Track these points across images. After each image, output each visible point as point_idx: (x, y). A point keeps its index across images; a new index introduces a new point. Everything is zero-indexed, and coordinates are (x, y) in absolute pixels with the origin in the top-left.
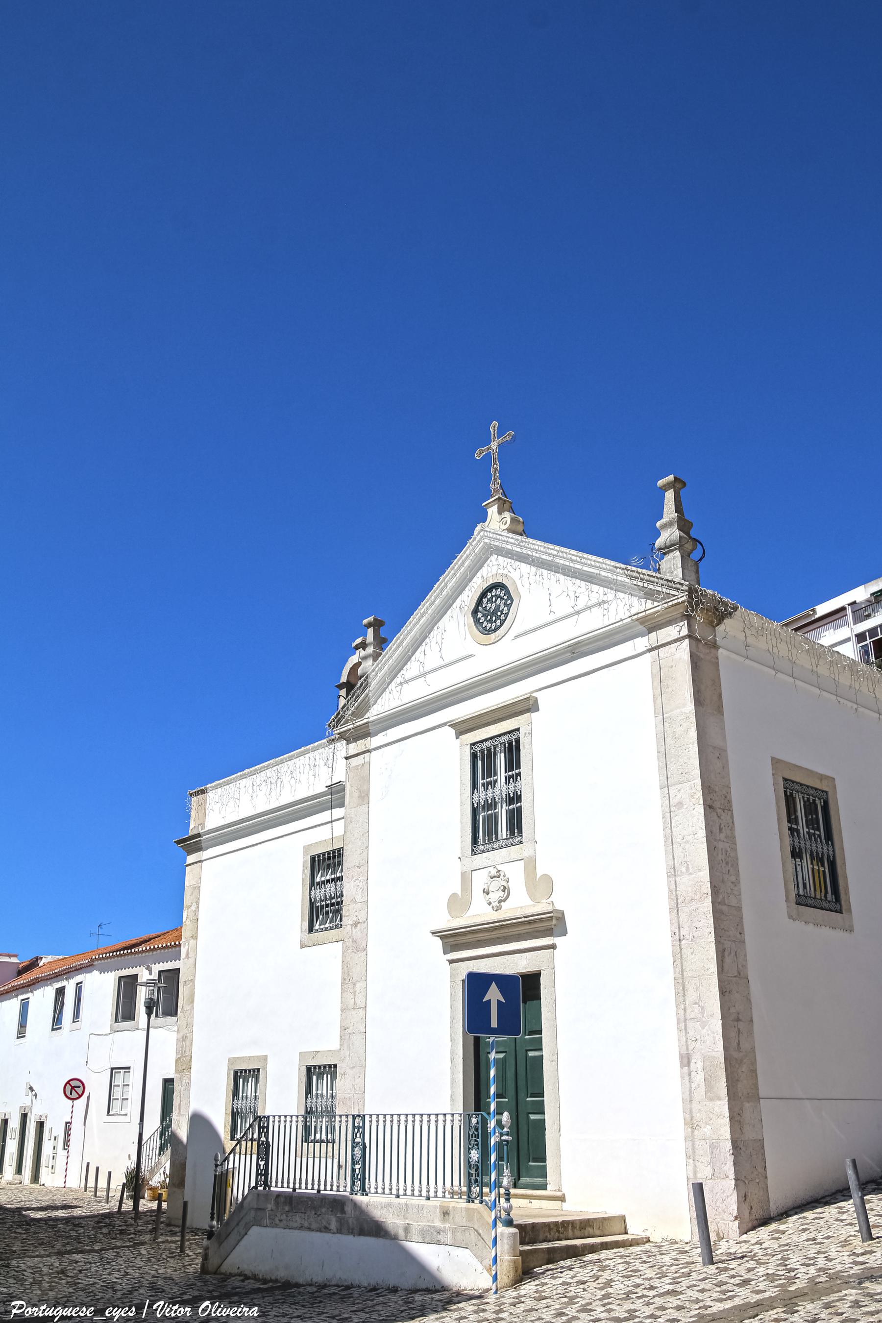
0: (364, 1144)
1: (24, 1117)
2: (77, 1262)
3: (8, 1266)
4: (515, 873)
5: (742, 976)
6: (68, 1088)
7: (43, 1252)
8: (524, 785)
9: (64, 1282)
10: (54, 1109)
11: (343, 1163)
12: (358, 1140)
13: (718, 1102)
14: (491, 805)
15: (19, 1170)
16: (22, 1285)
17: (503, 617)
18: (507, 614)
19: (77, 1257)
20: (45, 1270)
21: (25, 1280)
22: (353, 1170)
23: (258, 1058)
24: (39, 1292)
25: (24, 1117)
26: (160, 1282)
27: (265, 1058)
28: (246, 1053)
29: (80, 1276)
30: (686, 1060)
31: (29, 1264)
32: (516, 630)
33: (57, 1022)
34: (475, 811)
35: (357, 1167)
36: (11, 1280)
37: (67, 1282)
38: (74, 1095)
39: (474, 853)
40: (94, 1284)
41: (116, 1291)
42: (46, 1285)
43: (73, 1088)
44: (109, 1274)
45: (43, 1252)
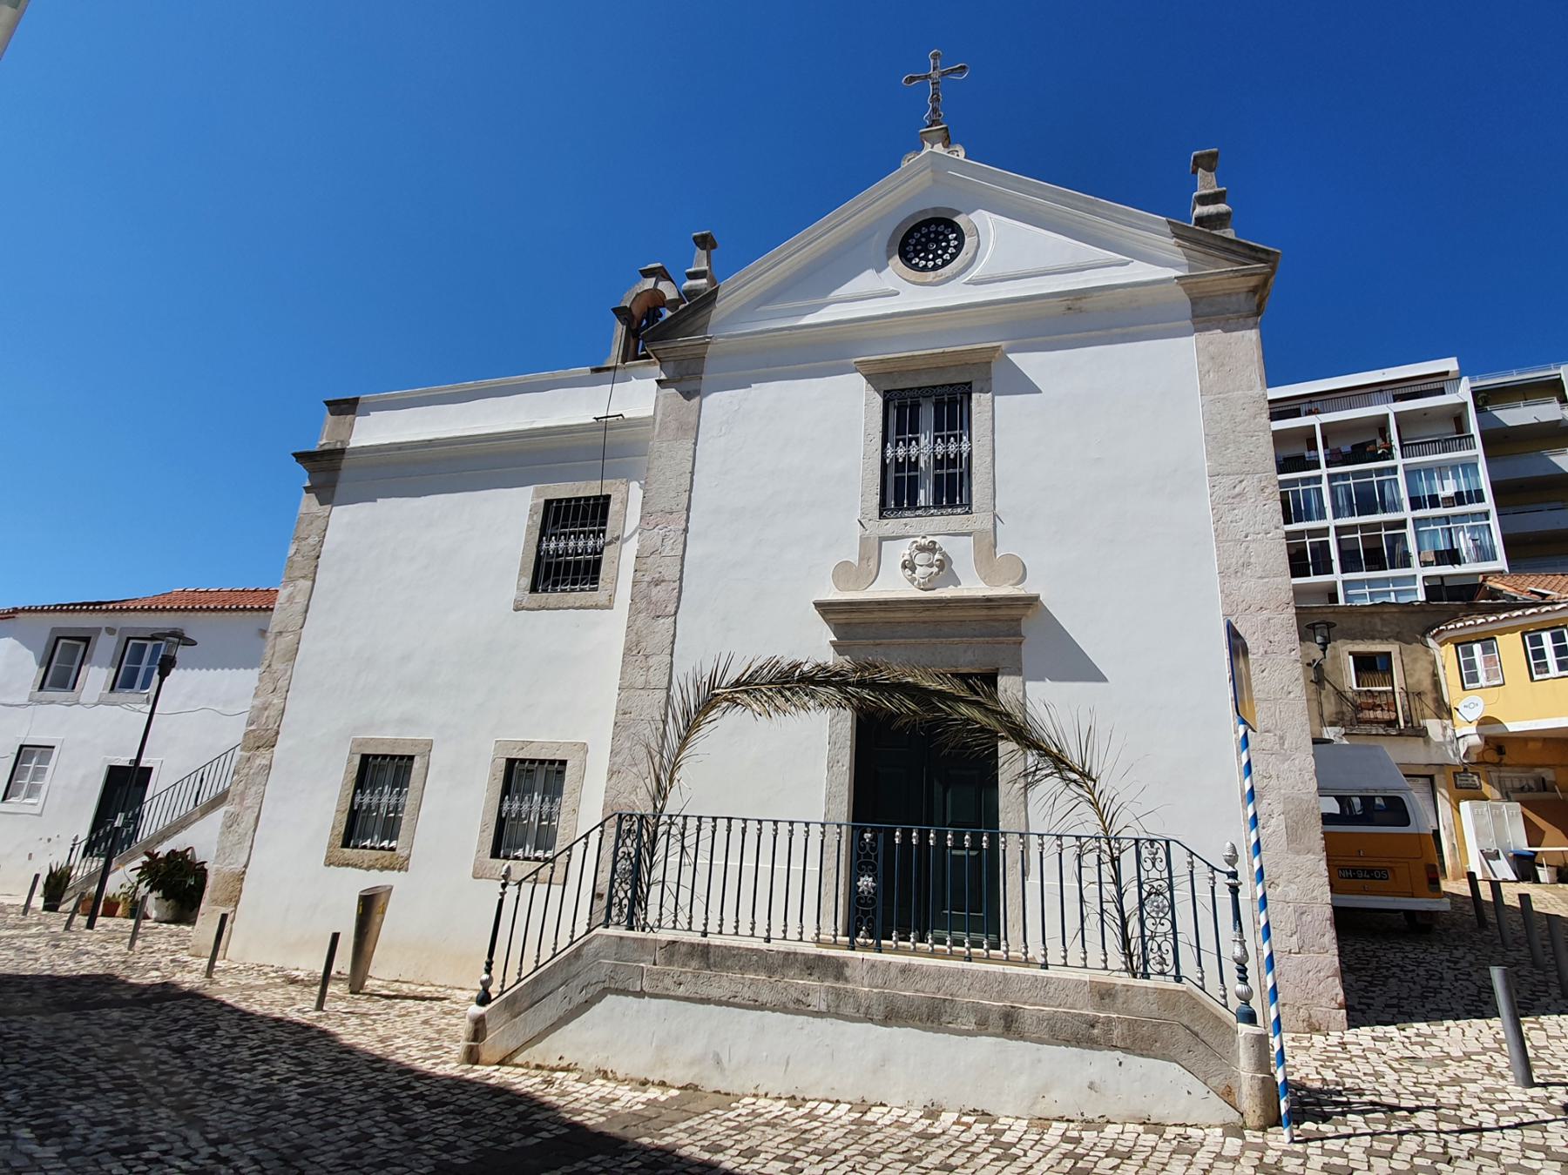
4: (961, 551)
23: (414, 743)
27: (430, 744)
28: (387, 736)
32: (976, 272)
39: (881, 516)
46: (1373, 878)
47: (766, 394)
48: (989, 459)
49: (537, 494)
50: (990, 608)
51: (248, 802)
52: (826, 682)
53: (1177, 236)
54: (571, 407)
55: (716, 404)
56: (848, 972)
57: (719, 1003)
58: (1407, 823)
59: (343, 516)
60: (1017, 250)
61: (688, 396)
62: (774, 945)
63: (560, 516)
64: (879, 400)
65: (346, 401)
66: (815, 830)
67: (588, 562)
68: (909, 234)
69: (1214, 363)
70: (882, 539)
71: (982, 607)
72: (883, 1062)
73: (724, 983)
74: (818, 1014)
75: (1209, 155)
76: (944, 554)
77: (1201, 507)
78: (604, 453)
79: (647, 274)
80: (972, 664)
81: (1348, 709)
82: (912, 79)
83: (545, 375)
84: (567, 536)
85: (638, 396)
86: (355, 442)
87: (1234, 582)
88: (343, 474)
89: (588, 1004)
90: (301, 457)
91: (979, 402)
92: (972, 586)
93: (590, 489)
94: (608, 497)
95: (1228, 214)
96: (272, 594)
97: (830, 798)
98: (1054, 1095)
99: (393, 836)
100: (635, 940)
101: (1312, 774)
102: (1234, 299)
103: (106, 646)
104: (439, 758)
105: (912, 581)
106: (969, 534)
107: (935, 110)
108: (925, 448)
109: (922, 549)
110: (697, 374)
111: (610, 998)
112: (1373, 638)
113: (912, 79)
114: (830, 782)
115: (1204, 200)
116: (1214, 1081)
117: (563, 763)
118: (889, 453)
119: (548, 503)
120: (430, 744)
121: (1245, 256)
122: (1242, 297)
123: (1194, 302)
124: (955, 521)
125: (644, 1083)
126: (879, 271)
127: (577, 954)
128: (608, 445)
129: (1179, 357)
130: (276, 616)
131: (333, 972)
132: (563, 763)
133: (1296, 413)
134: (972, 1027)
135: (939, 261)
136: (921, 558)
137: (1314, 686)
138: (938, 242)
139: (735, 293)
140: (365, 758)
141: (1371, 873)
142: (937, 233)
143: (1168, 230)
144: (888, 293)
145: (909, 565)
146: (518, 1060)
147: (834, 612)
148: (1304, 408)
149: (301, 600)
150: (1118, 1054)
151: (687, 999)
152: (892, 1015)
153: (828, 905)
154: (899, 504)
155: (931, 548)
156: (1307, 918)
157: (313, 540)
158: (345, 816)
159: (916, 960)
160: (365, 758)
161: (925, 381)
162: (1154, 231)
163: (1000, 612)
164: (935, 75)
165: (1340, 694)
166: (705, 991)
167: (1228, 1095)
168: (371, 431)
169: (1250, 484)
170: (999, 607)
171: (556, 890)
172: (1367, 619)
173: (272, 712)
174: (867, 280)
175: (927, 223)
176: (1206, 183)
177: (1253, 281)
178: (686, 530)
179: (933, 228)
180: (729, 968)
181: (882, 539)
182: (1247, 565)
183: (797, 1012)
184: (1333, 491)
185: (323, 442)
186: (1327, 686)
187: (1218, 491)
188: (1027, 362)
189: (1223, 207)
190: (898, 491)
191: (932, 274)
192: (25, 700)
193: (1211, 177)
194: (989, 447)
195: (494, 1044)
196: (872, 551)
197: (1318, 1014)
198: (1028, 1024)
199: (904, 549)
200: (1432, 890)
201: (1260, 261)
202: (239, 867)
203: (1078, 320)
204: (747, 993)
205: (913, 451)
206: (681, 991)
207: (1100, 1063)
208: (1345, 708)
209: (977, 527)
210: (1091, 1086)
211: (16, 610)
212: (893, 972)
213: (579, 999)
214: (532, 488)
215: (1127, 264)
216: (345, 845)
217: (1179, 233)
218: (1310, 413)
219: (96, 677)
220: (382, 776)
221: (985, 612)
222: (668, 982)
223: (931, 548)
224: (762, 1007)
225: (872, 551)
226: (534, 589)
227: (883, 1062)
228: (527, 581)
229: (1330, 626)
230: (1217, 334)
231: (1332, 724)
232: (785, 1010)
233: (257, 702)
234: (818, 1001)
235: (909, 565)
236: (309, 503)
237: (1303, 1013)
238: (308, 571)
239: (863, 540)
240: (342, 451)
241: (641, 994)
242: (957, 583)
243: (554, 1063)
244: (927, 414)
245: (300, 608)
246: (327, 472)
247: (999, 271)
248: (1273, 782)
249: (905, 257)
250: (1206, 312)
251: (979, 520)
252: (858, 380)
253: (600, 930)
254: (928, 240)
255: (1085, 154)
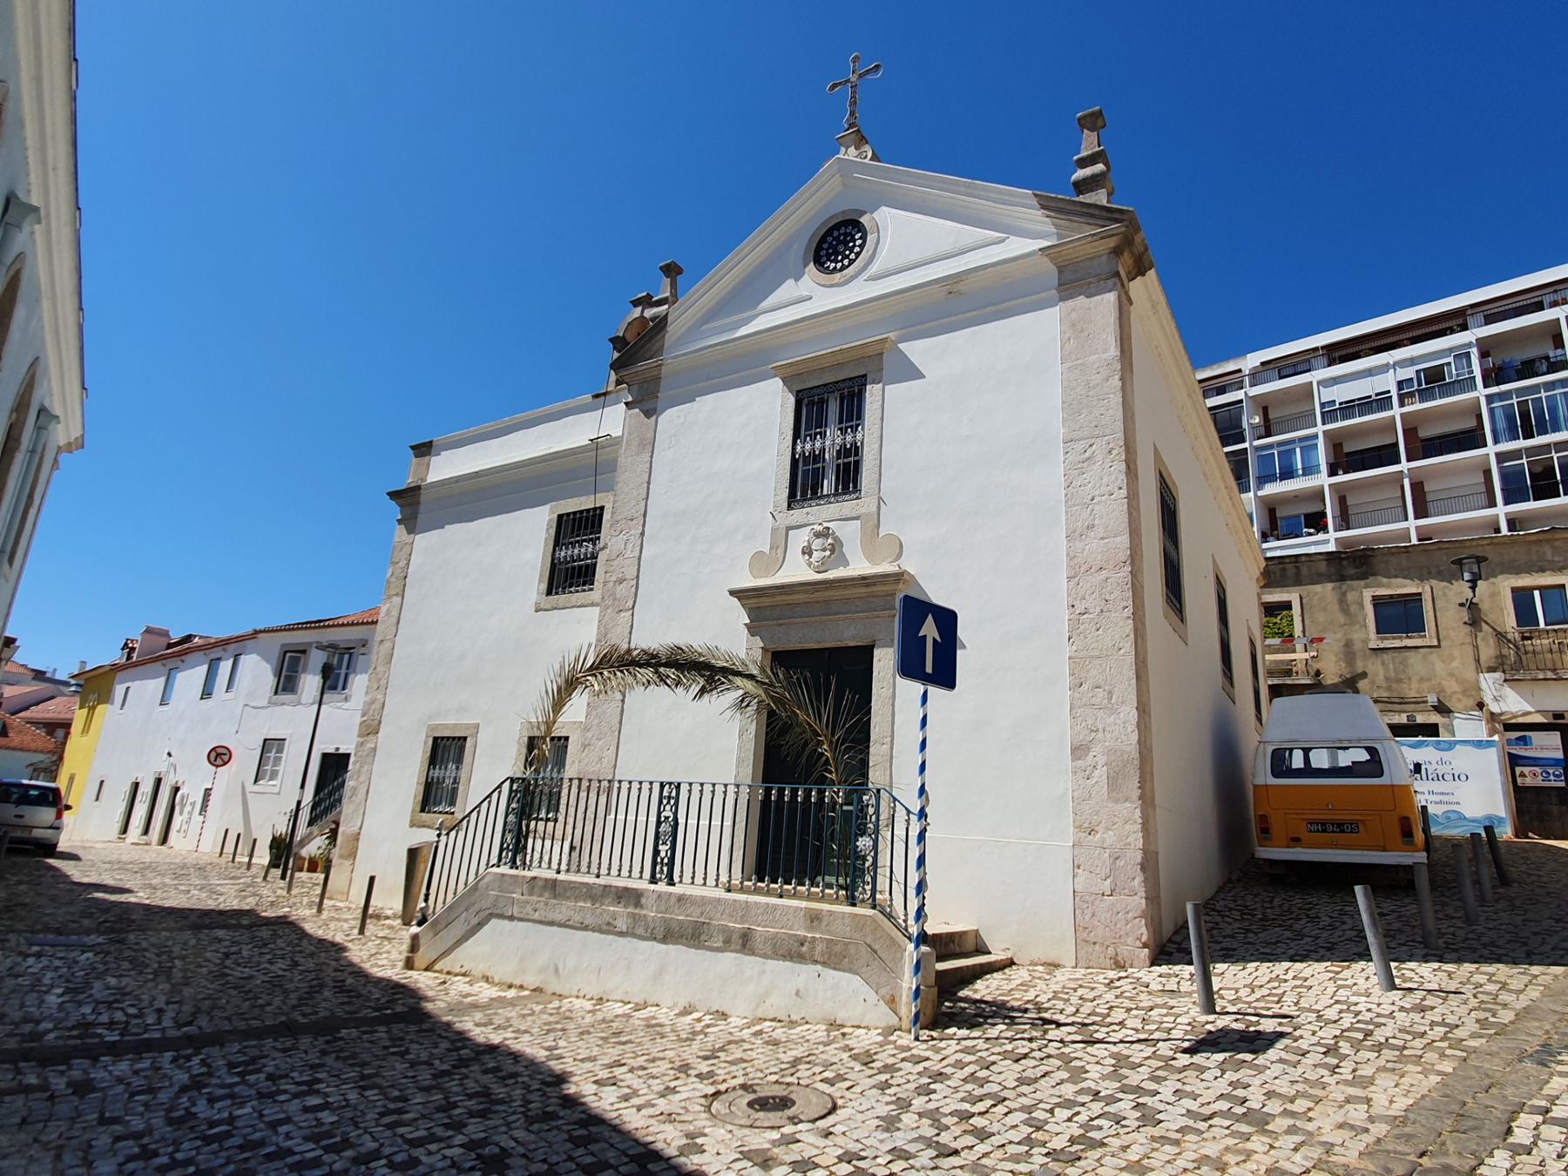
0: (676, 819)
1: (158, 781)
2: (220, 941)
3: (122, 942)
4: (849, 533)
5: (1144, 661)
6: (213, 755)
7: (172, 924)
8: (868, 435)
9: (204, 970)
10: (194, 777)
11: (577, 843)
12: (667, 813)
13: (1128, 805)
14: (817, 457)
15: (146, 832)
16: (141, 973)
17: (852, 256)
18: (858, 254)
19: (220, 933)
20: (176, 950)
21: (147, 966)
22: (656, 852)
23: (467, 726)
24: (167, 986)
25: (158, 781)
26: (350, 981)
27: (477, 726)
28: (450, 722)
29: (228, 962)
30: (1079, 751)
31: (153, 940)
32: (874, 269)
33: (207, 693)
34: (794, 463)
35: (663, 848)
36: (126, 965)
37: (210, 972)
38: (219, 762)
39: (789, 507)
40: (251, 977)
41: (286, 992)
42: (177, 975)
43: (218, 755)
44: (271, 962)
45: (172, 924)
46: (1343, 831)
47: (706, 403)
48: (877, 446)
49: (552, 511)
50: (867, 585)
51: (362, 778)
52: (647, 665)
53: (1043, 207)
54: (570, 434)
55: (670, 418)
56: (643, 900)
57: (560, 925)
58: (1381, 774)
59: (422, 541)
60: (913, 241)
61: (648, 413)
62: (562, 877)
63: (579, 528)
64: (792, 400)
65: (424, 445)
66: (731, 789)
67: (587, 566)
68: (823, 240)
69: (1075, 330)
70: (789, 528)
71: (861, 586)
72: (661, 972)
73: (563, 909)
74: (621, 934)
75: (1091, 115)
76: (836, 539)
77: (1051, 477)
78: (596, 469)
79: (636, 303)
80: (853, 638)
81: (1511, 653)
82: (834, 86)
83: (559, 406)
84: (580, 543)
85: (614, 420)
86: (432, 477)
87: (1079, 545)
88: (422, 507)
89: (480, 925)
90: (394, 495)
91: (872, 392)
92: (859, 565)
93: (584, 503)
94: (602, 508)
95: (1102, 175)
96: (377, 610)
97: (739, 762)
98: (772, 1000)
99: (452, 803)
100: (660, 895)
101: (1134, 727)
102: (1096, 262)
103: (317, 658)
104: (484, 738)
105: (810, 564)
106: (857, 518)
107: (852, 114)
108: (832, 439)
109: (818, 535)
110: (654, 395)
111: (494, 921)
112: (1542, 570)
113: (834, 86)
114: (740, 748)
115: (1084, 163)
116: (883, 991)
117: (567, 739)
118: (799, 449)
119: (560, 517)
120: (477, 726)
121: (1109, 219)
122: (1104, 259)
123: (1061, 270)
124: (847, 506)
125: (510, 986)
126: (797, 280)
127: (475, 887)
128: (596, 463)
129: (1042, 327)
130: (379, 627)
131: (370, 911)
132: (567, 739)
133: (1539, 307)
134: (720, 944)
135: (846, 262)
136: (817, 544)
137: (1468, 629)
138: (846, 243)
139: (681, 319)
140: (435, 739)
141: (1341, 827)
142: (846, 234)
143: (1034, 202)
144: (807, 298)
145: (808, 551)
146: (437, 967)
147: (748, 598)
148: (1547, 300)
149: (395, 613)
150: (819, 967)
151: (541, 922)
152: (669, 935)
153: (738, 855)
154: (804, 494)
155: (824, 534)
156: (1120, 863)
157: (403, 563)
158: (422, 788)
159: (825, 907)
160: (435, 739)
161: (829, 378)
162: (1022, 206)
163: (874, 589)
164: (853, 78)
165: (1500, 636)
166: (552, 916)
167: (892, 1002)
168: (444, 467)
169: (1099, 447)
170: (874, 584)
171: (548, 843)
172: (1534, 548)
173: (377, 706)
174: (788, 290)
175: (837, 226)
176: (1089, 144)
177: (1112, 242)
178: (643, 534)
179: (836, 234)
180: (568, 898)
181: (789, 528)
182: (1091, 527)
183: (608, 932)
184: (1492, 411)
185: (410, 481)
186: (1485, 627)
187: (1071, 458)
188: (914, 350)
189: (1100, 167)
190: (804, 483)
191: (838, 275)
192: (265, 703)
193: (1093, 136)
194: (877, 434)
195: (422, 958)
196: (781, 538)
197: (1124, 952)
198: (758, 942)
199: (801, 538)
200: (1406, 843)
201: (1117, 221)
202: (356, 829)
203: (960, 303)
204: (577, 918)
205: (818, 444)
206: (536, 916)
207: (805, 974)
208: (1505, 651)
209: (863, 511)
210: (797, 993)
211: (256, 632)
212: (673, 900)
213: (475, 921)
214: (548, 507)
215: (1003, 241)
216: (422, 810)
217: (1046, 204)
218: (1554, 304)
219: (310, 683)
220: (447, 750)
221: (863, 590)
222: (529, 908)
223: (824, 534)
224: (586, 928)
225: (781, 538)
226: (549, 593)
227: (661, 972)
228: (544, 586)
229: (1480, 560)
230: (1081, 300)
231: (1491, 670)
232: (601, 931)
233: (368, 698)
234: (622, 924)
235: (808, 551)
236: (400, 531)
237: (1111, 951)
238: (399, 590)
239: (774, 530)
240: (419, 488)
241: (511, 918)
242: (846, 564)
243: (458, 970)
244: (833, 409)
245: (394, 620)
246: (412, 505)
247: (892, 265)
248: (1100, 734)
249: (819, 263)
250: (1072, 279)
251: (863, 505)
252: (777, 383)
253: (495, 870)
254: (837, 243)
255: (959, 146)
